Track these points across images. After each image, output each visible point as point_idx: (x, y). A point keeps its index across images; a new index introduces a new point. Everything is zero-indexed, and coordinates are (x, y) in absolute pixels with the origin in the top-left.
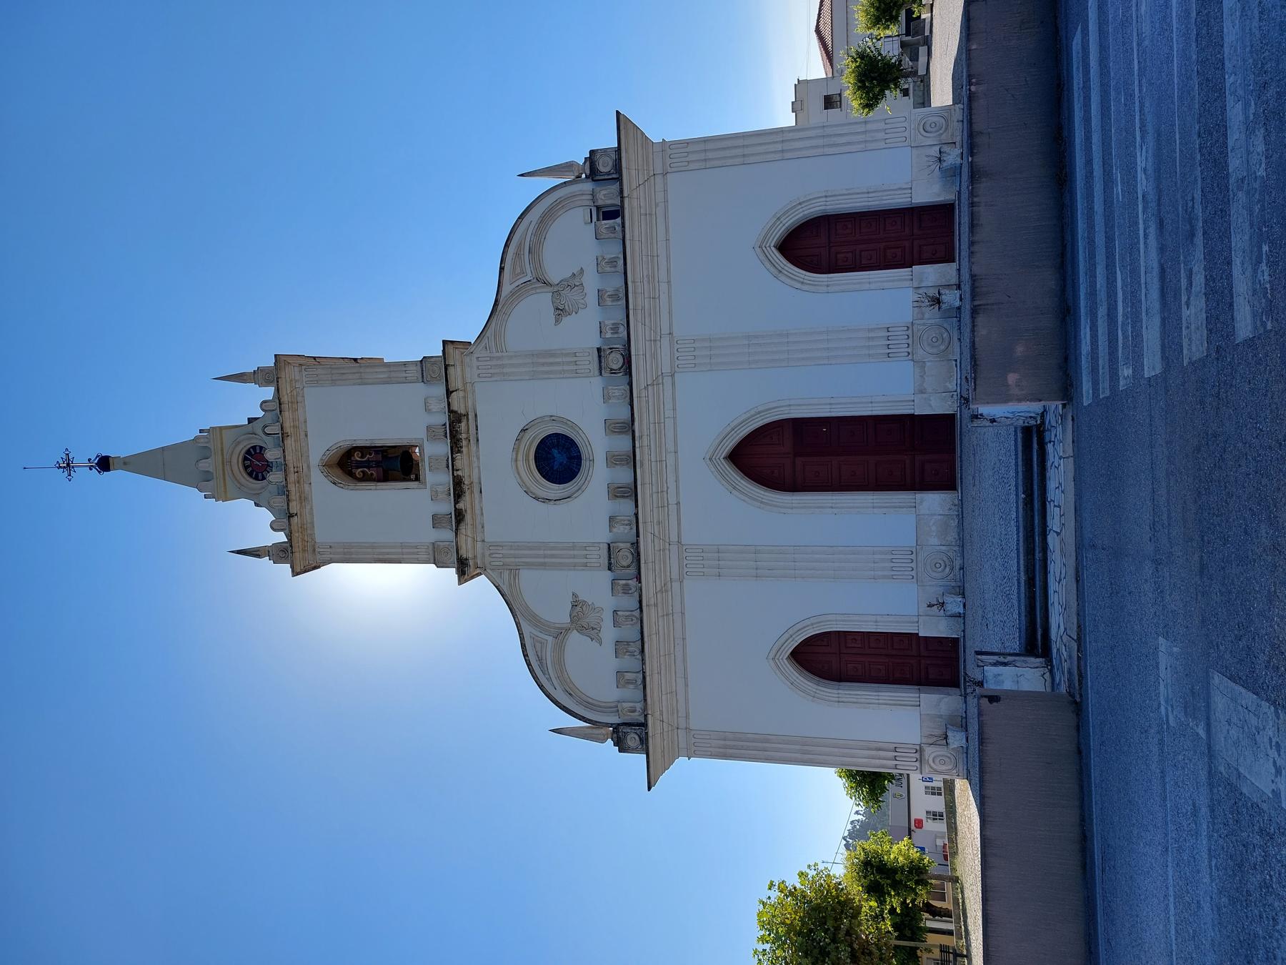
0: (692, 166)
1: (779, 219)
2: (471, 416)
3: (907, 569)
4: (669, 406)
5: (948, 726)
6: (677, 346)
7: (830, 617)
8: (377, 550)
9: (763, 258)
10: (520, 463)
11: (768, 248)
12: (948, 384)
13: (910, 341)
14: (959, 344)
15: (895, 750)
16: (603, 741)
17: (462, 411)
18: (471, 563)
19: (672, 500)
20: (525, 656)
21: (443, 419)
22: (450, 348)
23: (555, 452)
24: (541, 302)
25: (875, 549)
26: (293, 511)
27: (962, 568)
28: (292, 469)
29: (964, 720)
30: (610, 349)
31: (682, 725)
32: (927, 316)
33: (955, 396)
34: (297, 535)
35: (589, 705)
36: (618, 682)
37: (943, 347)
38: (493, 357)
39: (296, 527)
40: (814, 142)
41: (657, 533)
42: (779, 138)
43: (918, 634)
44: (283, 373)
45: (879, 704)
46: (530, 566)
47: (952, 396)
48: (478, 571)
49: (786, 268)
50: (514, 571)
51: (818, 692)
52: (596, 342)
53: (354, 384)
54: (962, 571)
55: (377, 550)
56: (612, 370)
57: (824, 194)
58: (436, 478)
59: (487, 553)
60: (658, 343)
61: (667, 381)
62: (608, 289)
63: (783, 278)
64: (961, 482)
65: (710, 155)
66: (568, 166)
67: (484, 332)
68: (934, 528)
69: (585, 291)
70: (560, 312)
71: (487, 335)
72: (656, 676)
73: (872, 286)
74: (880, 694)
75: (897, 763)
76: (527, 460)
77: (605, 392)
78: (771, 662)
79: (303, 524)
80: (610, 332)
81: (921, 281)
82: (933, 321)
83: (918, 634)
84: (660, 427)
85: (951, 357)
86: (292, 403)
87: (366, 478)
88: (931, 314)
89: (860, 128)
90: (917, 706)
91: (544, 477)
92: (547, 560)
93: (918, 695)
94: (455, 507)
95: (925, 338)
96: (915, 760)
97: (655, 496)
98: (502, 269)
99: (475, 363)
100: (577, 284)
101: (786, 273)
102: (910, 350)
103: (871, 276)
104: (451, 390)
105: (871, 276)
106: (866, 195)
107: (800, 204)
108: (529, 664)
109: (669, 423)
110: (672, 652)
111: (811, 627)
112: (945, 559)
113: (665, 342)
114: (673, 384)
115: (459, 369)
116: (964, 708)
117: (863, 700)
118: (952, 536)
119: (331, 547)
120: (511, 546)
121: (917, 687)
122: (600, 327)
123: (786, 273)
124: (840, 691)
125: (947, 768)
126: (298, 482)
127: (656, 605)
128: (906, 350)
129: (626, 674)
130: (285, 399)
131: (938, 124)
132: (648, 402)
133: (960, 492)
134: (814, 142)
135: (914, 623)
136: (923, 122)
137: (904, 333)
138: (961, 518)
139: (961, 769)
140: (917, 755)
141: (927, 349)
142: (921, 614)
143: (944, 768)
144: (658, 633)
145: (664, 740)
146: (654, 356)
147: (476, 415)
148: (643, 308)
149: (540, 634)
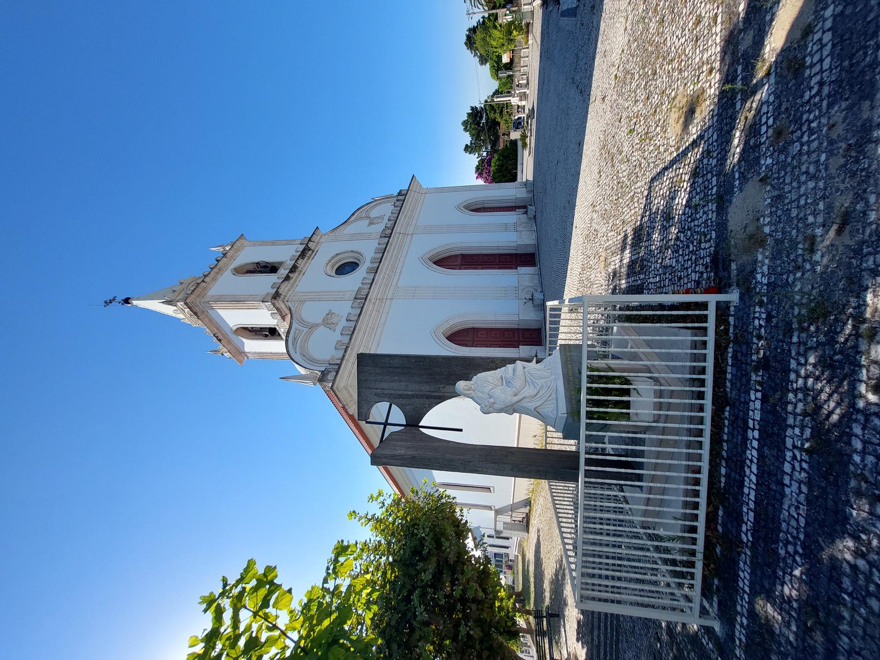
18: (282, 297)
69: (360, 285)
70: (371, 224)
118: (536, 281)
127: (374, 304)
148: (406, 215)
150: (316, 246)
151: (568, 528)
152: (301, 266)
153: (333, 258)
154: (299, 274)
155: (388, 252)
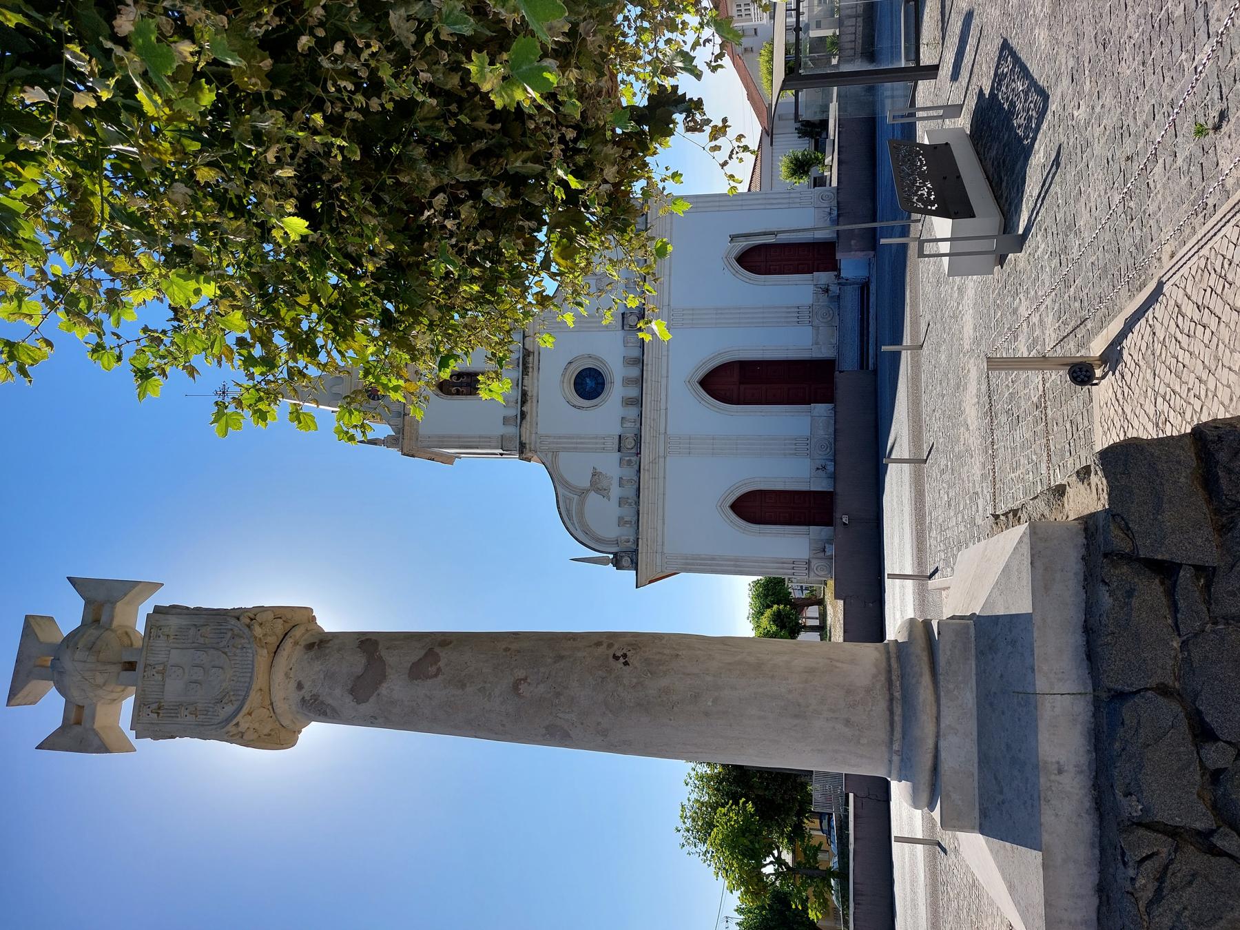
10: (565, 384)
18: (528, 447)
19: (663, 407)
50: (555, 453)
73: (790, 283)
88: (824, 298)
118: (831, 430)
140: (807, 566)
143: (823, 573)
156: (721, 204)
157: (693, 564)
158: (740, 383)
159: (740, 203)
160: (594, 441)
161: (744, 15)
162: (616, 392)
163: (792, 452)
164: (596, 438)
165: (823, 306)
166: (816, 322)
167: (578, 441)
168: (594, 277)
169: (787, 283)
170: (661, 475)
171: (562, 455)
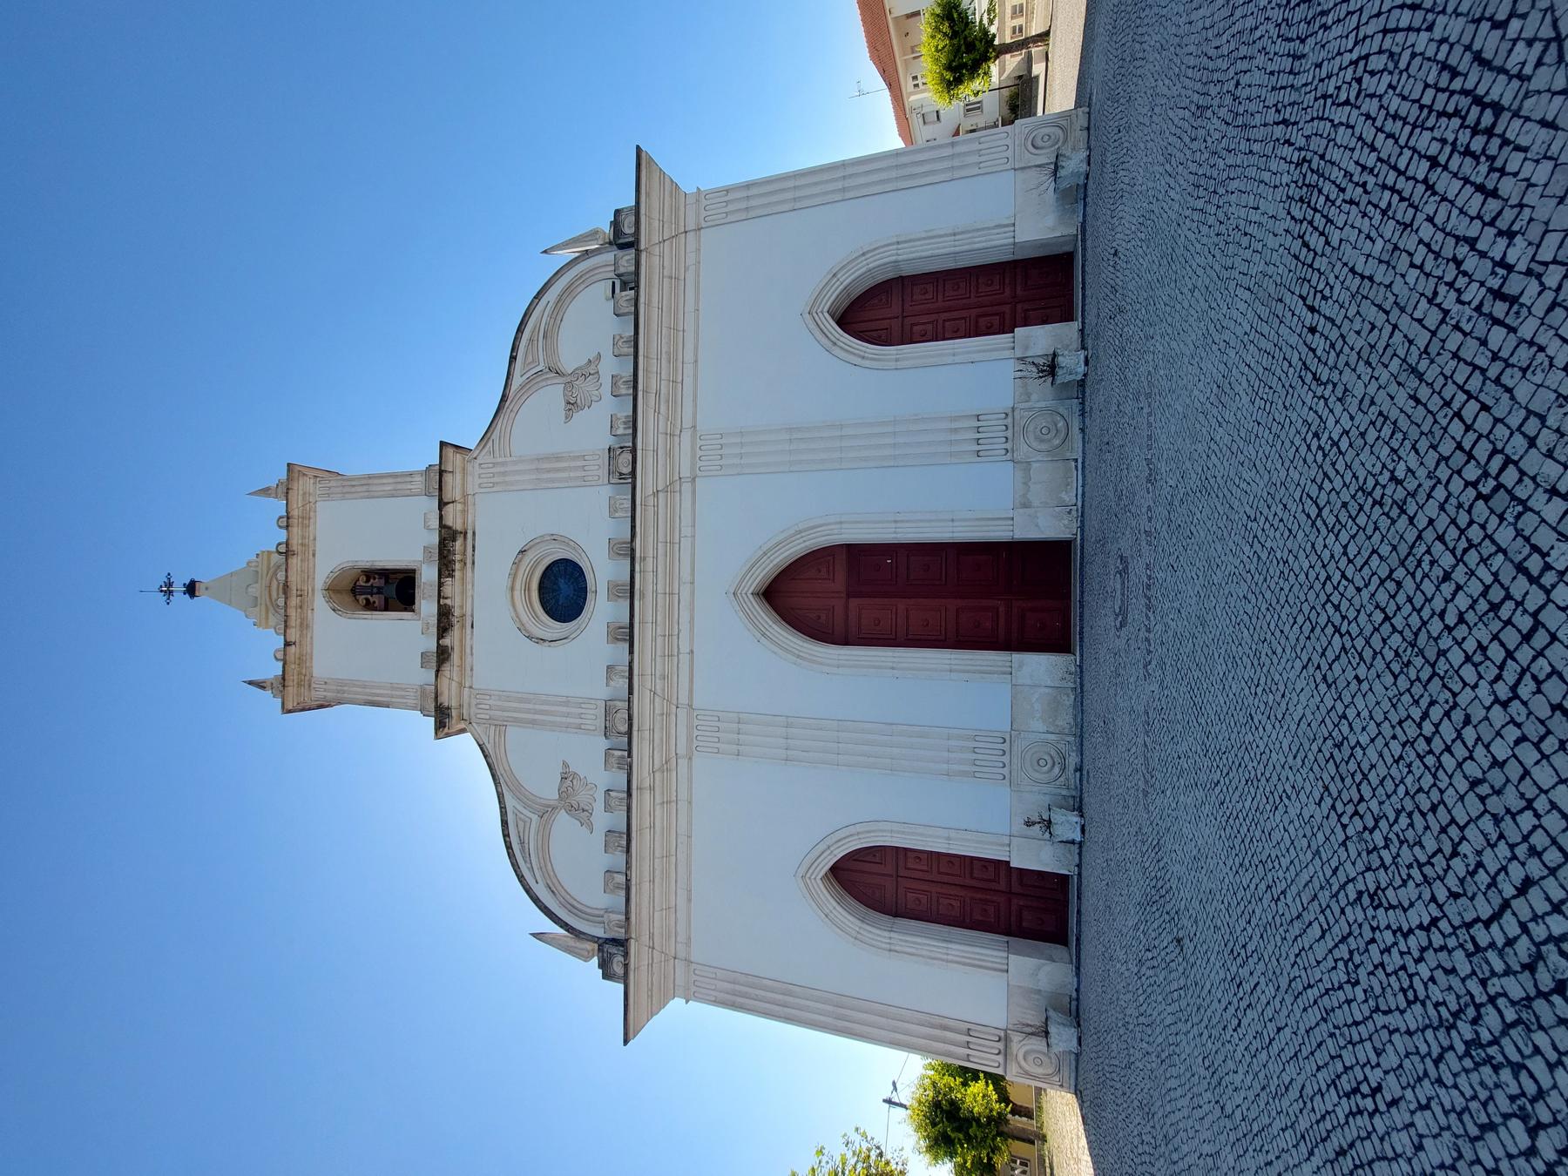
0: (731, 218)
1: (834, 275)
2: (470, 535)
3: (997, 764)
4: (687, 520)
5: (1051, 1013)
6: (699, 443)
7: (881, 826)
8: (368, 690)
9: (812, 326)
10: (517, 593)
11: (820, 314)
12: (1063, 495)
13: (1009, 434)
14: (1081, 436)
15: (968, 1032)
16: (587, 959)
17: (459, 527)
18: (454, 713)
19: (685, 648)
20: (506, 835)
21: (434, 539)
22: (450, 452)
23: (562, 582)
24: (551, 396)
25: (951, 731)
26: (291, 638)
27: (1079, 769)
28: (295, 592)
29: (1074, 1003)
30: (621, 448)
31: (681, 954)
32: (1034, 397)
33: (1074, 513)
34: (293, 666)
35: (573, 909)
36: (606, 884)
37: (1057, 442)
38: (498, 463)
39: (293, 658)
40: (884, 176)
41: (659, 691)
42: (840, 174)
43: (1008, 862)
44: (296, 484)
45: (947, 961)
46: (518, 721)
47: (1069, 513)
48: (462, 725)
49: (841, 339)
50: (501, 726)
51: (862, 931)
52: (609, 441)
53: (362, 498)
54: (1078, 774)
55: (368, 690)
56: (621, 474)
57: (895, 240)
58: (427, 606)
59: (474, 702)
60: (677, 439)
61: (687, 487)
62: (623, 374)
63: (837, 351)
64: (1081, 639)
65: (753, 203)
66: (593, 234)
67: (489, 434)
68: (1037, 706)
71: (493, 437)
72: (646, 886)
73: (957, 359)
74: (950, 946)
75: (969, 1052)
76: (528, 589)
77: (612, 502)
78: (800, 880)
79: (301, 655)
80: (622, 426)
81: (1026, 348)
82: (1043, 404)
83: (1008, 862)
84: (672, 550)
85: (1068, 455)
86: (303, 518)
87: (369, 606)
88: (1041, 393)
89: (948, 152)
90: (1002, 971)
91: (547, 613)
92: (537, 717)
93: (1005, 955)
94: (438, 642)
95: (1031, 428)
96: (997, 1052)
97: (659, 640)
98: (513, 359)
99: (478, 471)
100: (592, 372)
101: (842, 345)
102: (1008, 446)
103: (956, 346)
104: (446, 500)
105: (956, 346)
106: (953, 238)
107: (863, 254)
108: (509, 847)
109: (686, 543)
110: (673, 852)
111: (856, 837)
112: (1053, 753)
113: (686, 437)
114: (694, 492)
115: (458, 476)
116: (1075, 983)
117: (924, 953)
118: (1065, 720)
119: (326, 683)
120: (499, 696)
121: (1006, 938)
122: (1513, 1137)
123: (842, 345)
124: (892, 935)
125: (1044, 1072)
126: (301, 607)
127: (652, 788)
128: (1004, 446)
129: (615, 875)
130: (295, 513)
131: (1053, 137)
132: (656, 514)
133: (1078, 654)
134: (884, 176)
135: (1003, 845)
136: (1031, 138)
137: (1000, 422)
138: (1080, 692)
139: (1066, 1074)
140: (1001, 1046)
141: (1035, 444)
142: (1015, 833)
143: (1039, 1071)
144: (652, 826)
145: (652, 974)
146: (669, 454)
147: (474, 533)
148: (658, 393)
149: (525, 811)
150: (464, 512)
151: (835, 180)
152: (457, 604)
153: (514, 576)
154: (463, 627)
155: (642, 596)
156: (798, 194)
157: (745, 996)
158: (849, 595)
159: (840, 185)
160: (564, 709)
161: (920, 85)
162: (601, 610)
163: (962, 768)
164: (566, 704)
165: (1041, 410)
166: (1023, 451)
167: (537, 707)
168: (561, 380)
169: (950, 360)
170: (683, 795)
171: (513, 732)
